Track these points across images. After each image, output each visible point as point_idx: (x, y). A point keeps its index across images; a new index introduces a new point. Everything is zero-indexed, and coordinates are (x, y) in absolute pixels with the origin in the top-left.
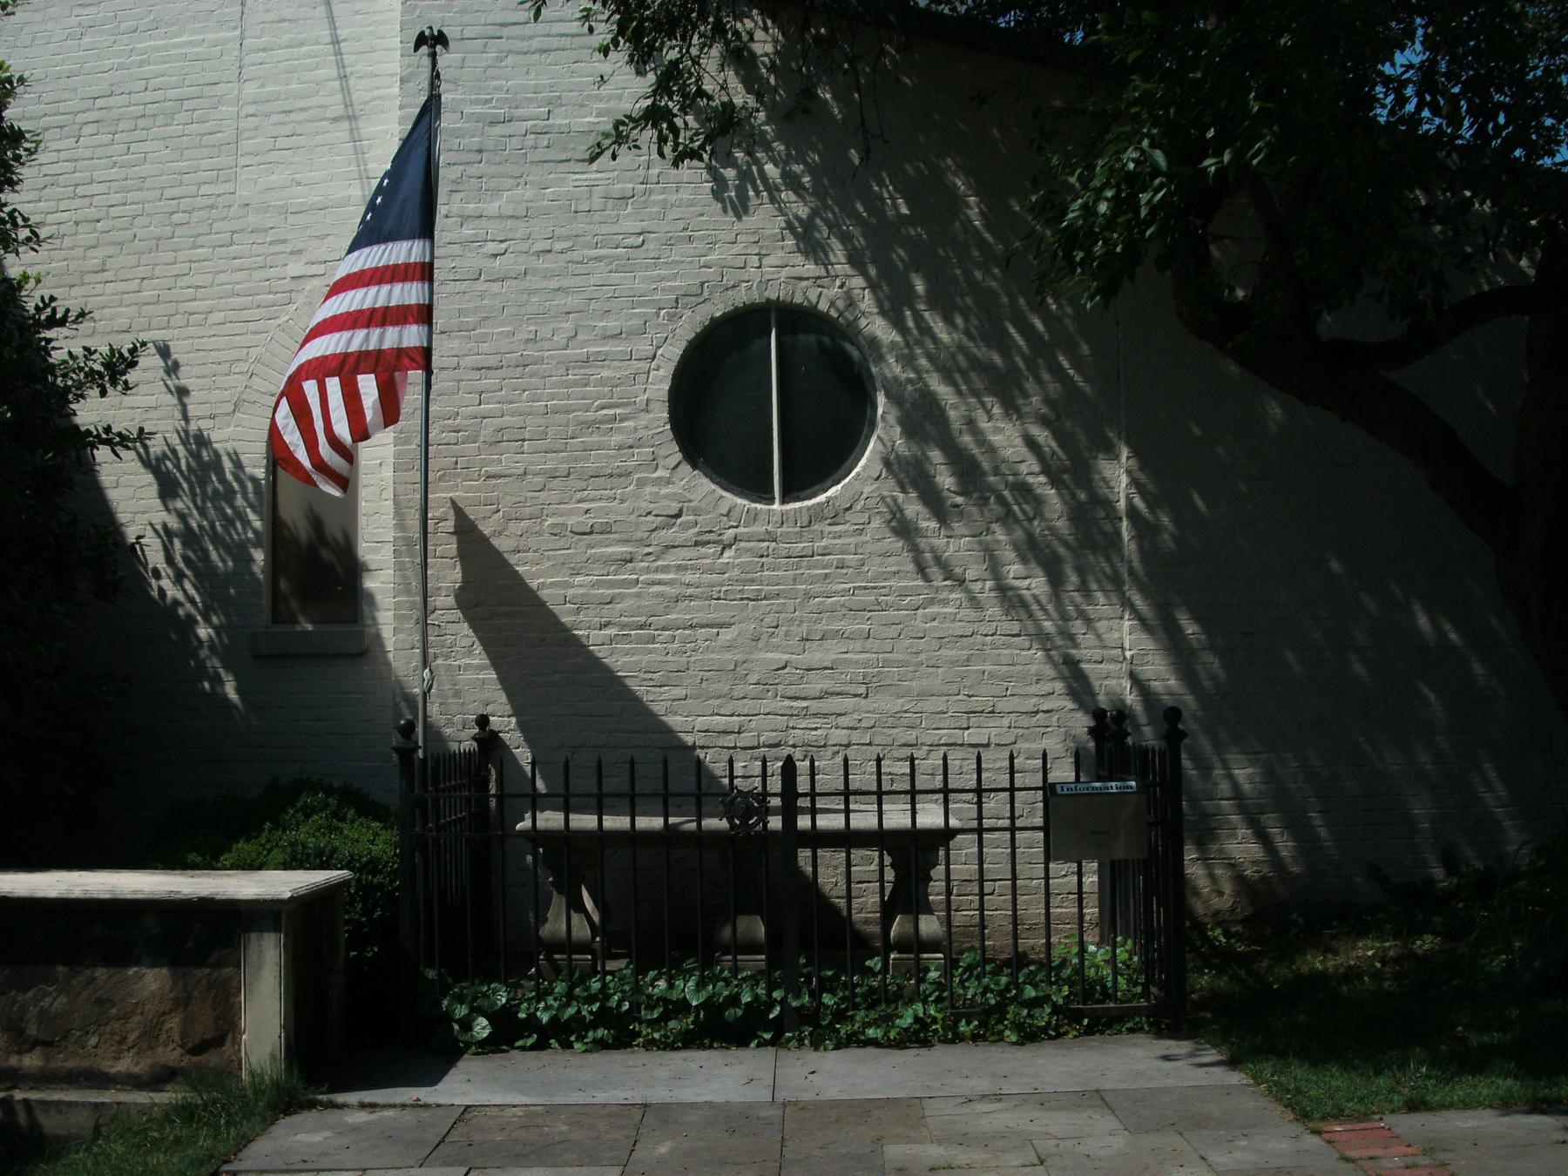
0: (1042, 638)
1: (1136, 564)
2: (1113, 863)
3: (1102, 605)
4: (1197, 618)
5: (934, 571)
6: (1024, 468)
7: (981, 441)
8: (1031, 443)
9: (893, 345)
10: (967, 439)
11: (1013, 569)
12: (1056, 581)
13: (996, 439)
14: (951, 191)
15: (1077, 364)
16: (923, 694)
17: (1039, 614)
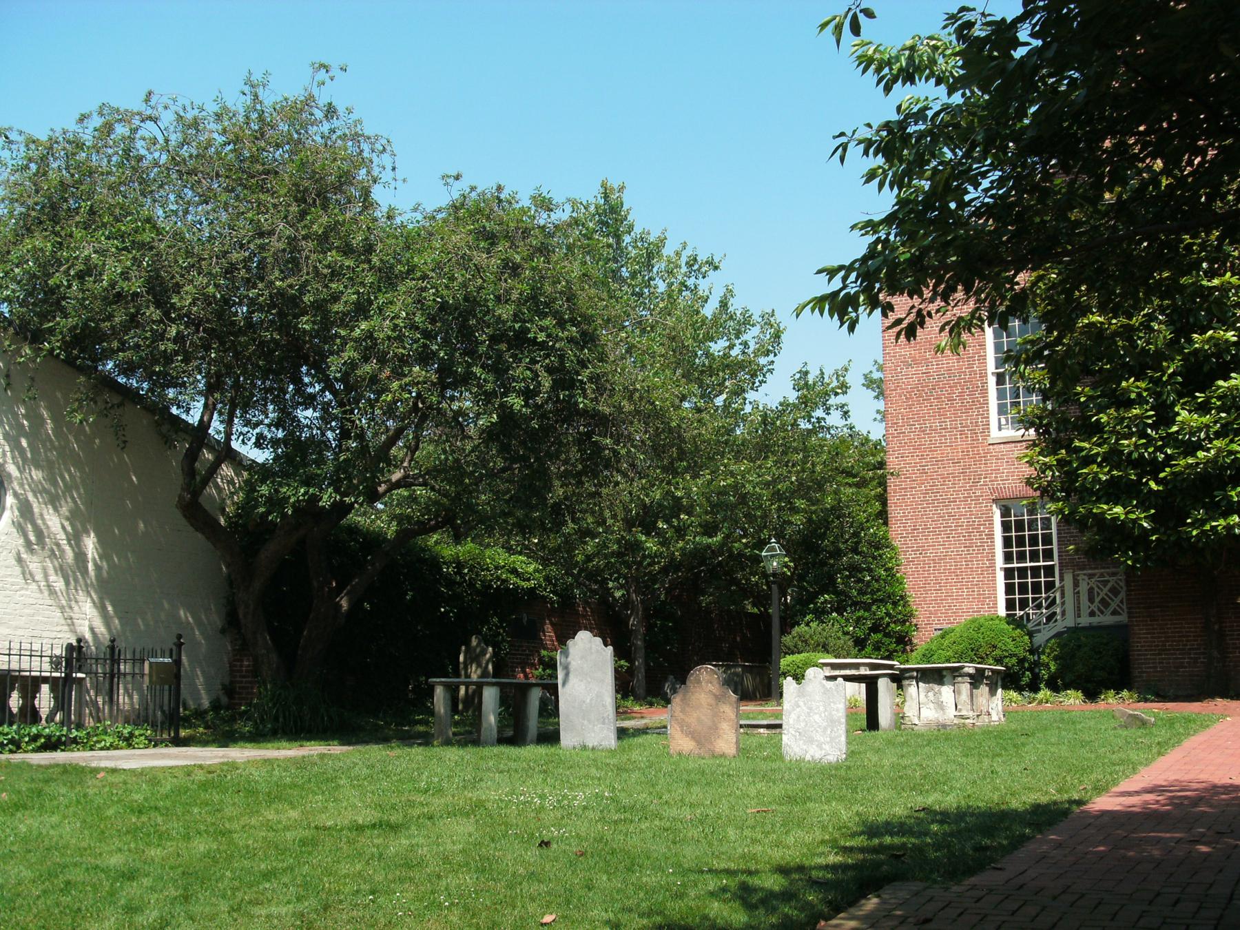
0: (62, 608)
1: (93, 578)
2: (665, 727)
3: (81, 596)
4: (113, 606)
5: (28, 576)
6: (58, 537)
7: (45, 524)
8: (63, 528)
9: (16, 478)
10: (39, 522)
11: (52, 578)
12: (67, 584)
13: (49, 523)
14: (42, 417)
15: (79, 494)
16: (17, 628)
17: (61, 598)
